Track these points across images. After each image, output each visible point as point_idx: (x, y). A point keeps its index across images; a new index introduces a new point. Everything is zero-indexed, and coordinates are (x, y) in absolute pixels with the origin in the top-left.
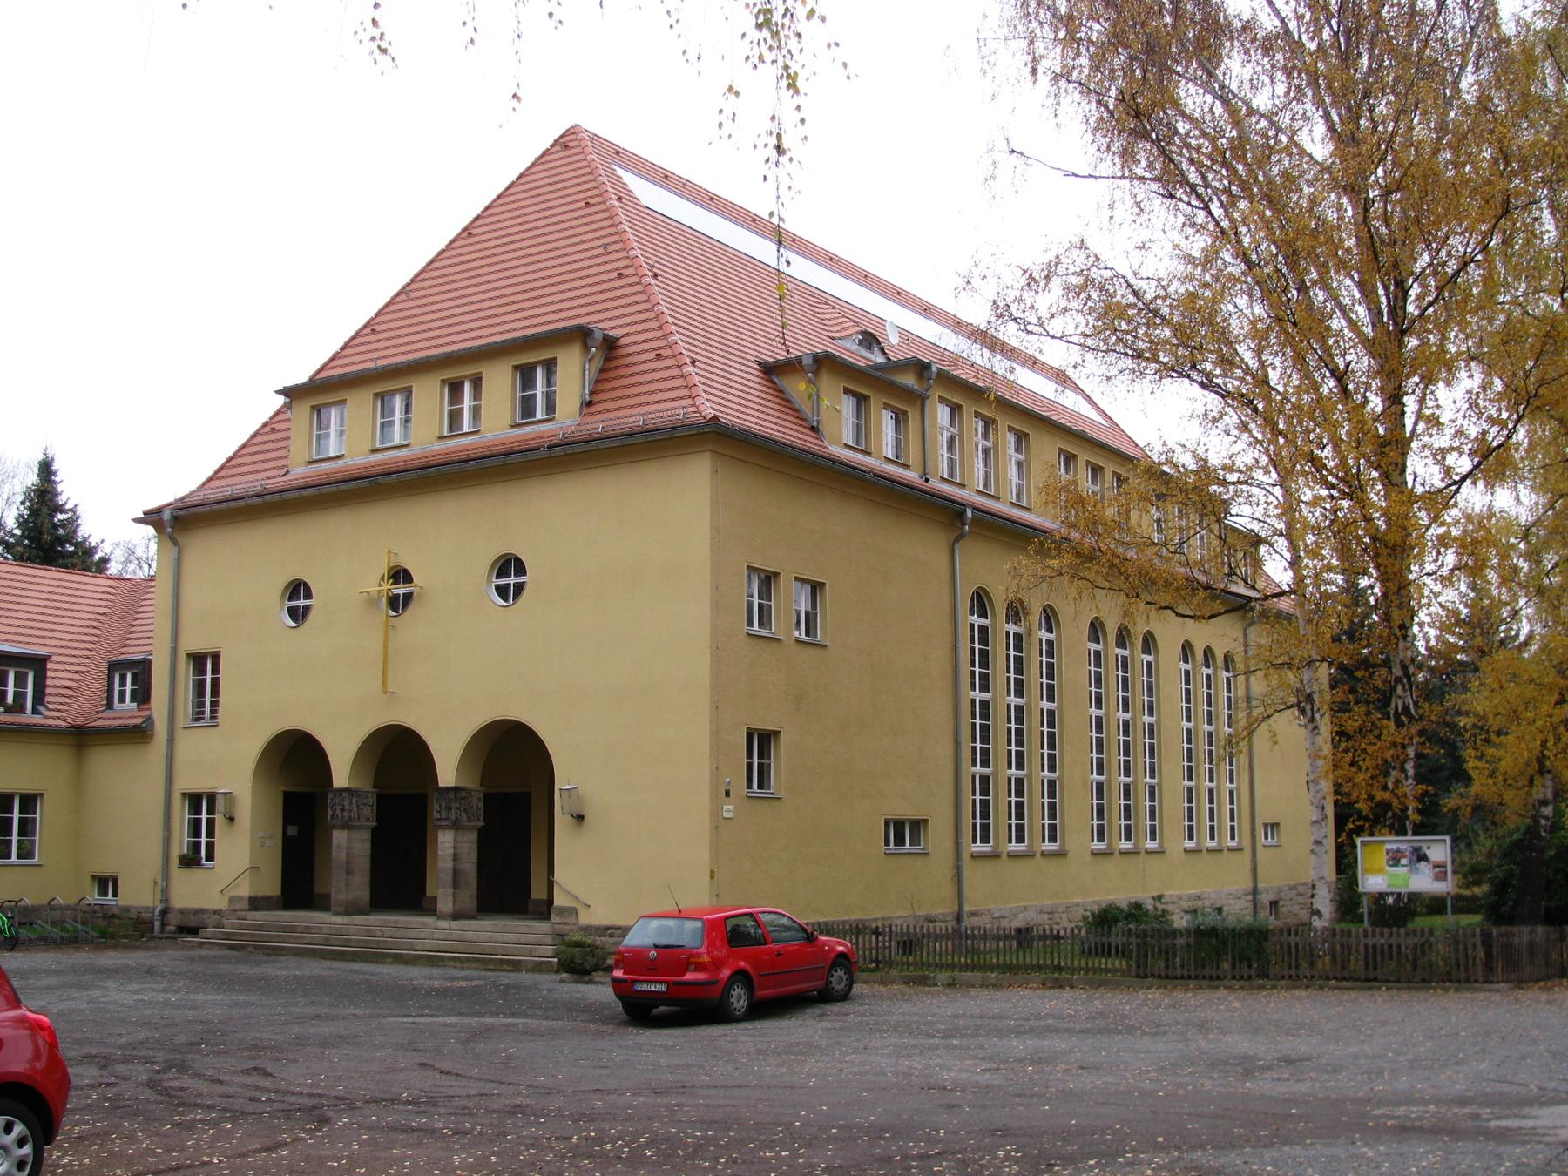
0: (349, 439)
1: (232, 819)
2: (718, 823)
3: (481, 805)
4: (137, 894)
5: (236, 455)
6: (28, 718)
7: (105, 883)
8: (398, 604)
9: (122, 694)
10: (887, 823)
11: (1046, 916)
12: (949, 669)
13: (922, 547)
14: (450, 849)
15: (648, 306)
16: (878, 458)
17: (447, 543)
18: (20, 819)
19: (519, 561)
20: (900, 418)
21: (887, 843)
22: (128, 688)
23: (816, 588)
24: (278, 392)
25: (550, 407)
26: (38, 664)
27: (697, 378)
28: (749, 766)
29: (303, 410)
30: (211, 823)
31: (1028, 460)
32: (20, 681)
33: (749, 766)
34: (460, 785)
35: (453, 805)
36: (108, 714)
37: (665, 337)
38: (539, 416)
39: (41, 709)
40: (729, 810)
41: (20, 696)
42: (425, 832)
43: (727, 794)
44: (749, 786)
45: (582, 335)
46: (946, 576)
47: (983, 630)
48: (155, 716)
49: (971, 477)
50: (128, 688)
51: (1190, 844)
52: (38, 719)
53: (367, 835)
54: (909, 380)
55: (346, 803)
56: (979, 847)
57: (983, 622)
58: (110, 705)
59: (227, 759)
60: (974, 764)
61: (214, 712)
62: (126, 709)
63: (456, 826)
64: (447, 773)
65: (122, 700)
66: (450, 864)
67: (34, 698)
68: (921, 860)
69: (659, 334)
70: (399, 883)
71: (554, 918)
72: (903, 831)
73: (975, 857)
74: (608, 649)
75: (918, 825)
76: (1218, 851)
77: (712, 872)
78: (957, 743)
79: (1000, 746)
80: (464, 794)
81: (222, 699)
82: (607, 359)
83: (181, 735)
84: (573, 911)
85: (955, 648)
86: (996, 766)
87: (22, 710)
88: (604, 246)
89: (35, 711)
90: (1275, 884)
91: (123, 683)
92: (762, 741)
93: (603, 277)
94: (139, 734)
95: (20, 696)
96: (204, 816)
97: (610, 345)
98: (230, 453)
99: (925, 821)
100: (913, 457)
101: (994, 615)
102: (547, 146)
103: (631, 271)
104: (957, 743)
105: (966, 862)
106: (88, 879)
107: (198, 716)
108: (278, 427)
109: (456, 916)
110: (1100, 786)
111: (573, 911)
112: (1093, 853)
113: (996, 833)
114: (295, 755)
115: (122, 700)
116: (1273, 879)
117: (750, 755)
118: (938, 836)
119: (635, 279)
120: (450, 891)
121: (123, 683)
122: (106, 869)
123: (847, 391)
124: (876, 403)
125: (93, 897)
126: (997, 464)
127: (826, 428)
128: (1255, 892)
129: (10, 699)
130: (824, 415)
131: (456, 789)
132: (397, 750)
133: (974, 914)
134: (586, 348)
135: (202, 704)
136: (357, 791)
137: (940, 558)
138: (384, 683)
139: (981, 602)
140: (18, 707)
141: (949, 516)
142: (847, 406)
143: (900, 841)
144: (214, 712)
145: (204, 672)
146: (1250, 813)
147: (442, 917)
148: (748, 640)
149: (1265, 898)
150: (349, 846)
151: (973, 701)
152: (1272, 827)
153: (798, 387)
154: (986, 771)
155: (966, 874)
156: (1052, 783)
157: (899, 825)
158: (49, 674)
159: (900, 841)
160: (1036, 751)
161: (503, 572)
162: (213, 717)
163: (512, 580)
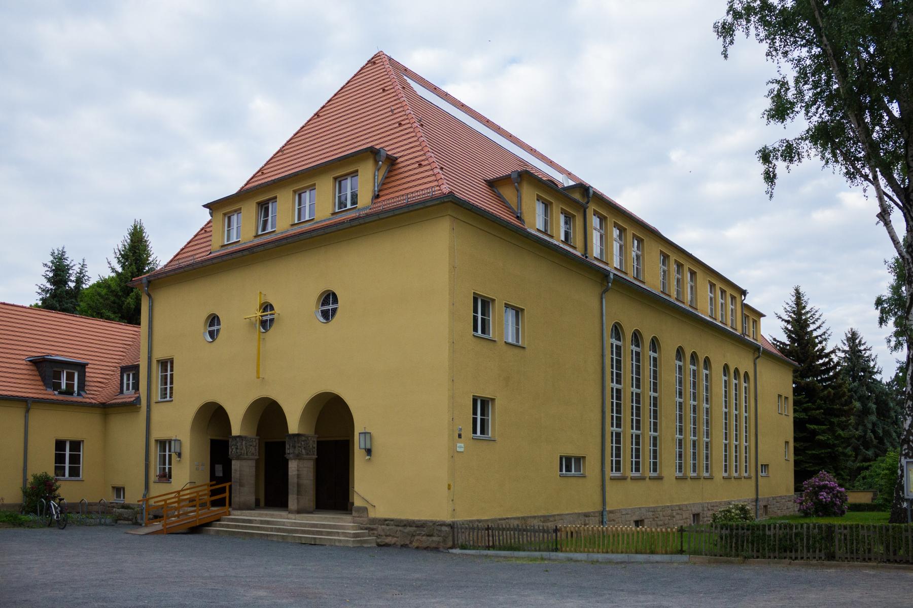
0: (244, 229)
1: (369, 452)
2: (454, 454)
3: (315, 446)
4: (133, 496)
5: (186, 247)
6: (75, 398)
7: (119, 491)
8: (266, 324)
9: (128, 385)
10: (561, 458)
11: (651, 513)
12: (599, 370)
13: (583, 295)
14: (300, 470)
15: (416, 139)
16: (558, 240)
17: (292, 287)
18: (70, 455)
19: (334, 295)
20: (569, 219)
21: (561, 470)
22: (131, 382)
23: (518, 312)
24: (204, 206)
25: (354, 202)
26: (81, 367)
27: (443, 177)
28: (475, 420)
29: (219, 215)
30: (170, 456)
31: (643, 255)
32: (70, 377)
33: (475, 420)
34: (301, 432)
35: (297, 445)
36: (121, 396)
37: (425, 154)
38: (349, 206)
39: (82, 393)
40: (460, 447)
41: (70, 386)
42: (295, 461)
43: (460, 436)
44: (475, 432)
45: (373, 153)
46: (597, 314)
47: (618, 348)
48: (142, 396)
49: (612, 259)
50: (131, 382)
51: (726, 475)
52: (80, 399)
53: (252, 463)
54: (577, 196)
55: (239, 444)
56: (615, 474)
57: (619, 343)
58: (122, 392)
59: (176, 420)
60: (612, 426)
61: (171, 393)
62: (129, 395)
63: (298, 457)
64: (294, 426)
65: (128, 389)
66: (295, 480)
67: (78, 387)
68: (581, 481)
69: (422, 153)
70: (275, 495)
71: (354, 514)
72: (569, 463)
73: (612, 479)
74: (388, 346)
75: (579, 460)
76: (739, 478)
77: (449, 485)
78: (603, 412)
79: (627, 416)
80: (303, 438)
81: (174, 386)
82: (390, 171)
83: (155, 409)
84: (364, 510)
85: (603, 356)
86: (625, 426)
87: (71, 393)
88: (392, 111)
89: (79, 394)
90: (766, 496)
91: (128, 379)
92: (482, 405)
93: (406, 142)
94: (133, 406)
95: (70, 386)
96: (167, 453)
97: (392, 161)
98: (182, 246)
99: (584, 458)
100: (578, 241)
101: (624, 339)
102: (364, 64)
103: (427, 162)
104: (603, 412)
105: (608, 482)
106: (111, 489)
107: (164, 395)
108: (208, 230)
109: (299, 512)
110: (680, 441)
111: (364, 510)
112: (676, 478)
113: (624, 466)
114: (213, 415)
115: (128, 389)
116: (765, 493)
117: (475, 413)
118: (592, 467)
119: (409, 125)
120: (295, 496)
121: (128, 379)
122: (119, 484)
123: (539, 198)
124: (556, 208)
125: (111, 498)
126: (626, 253)
127: (526, 217)
128: (757, 500)
129: (64, 387)
130: (525, 208)
131: (298, 435)
132: (268, 413)
133: (611, 512)
134: (376, 162)
135: (166, 389)
136: (245, 437)
137: (594, 302)
138: (258, 372)
139: (617, 331)
140: (69, 391)
141: (600, 277)
142: (539, 208)
143: (568, 469)
144: (171, 393)
145: (166, 371)
146: (374, 545)
147: (291, 512)
148: (474, 339)
149: (761, 504)
150: (244, 469)
151: (612, 389)
152: (765, 467)
153: (508, 193)
154: (618, 430)
155: (607, 489)
156: (655, 438)
157: (568, 459)
158: (87, 374)
159: (568, 469)
160: (647, 419)
161: (325, 302)
162: (171, 397)
163: (330, 307)
